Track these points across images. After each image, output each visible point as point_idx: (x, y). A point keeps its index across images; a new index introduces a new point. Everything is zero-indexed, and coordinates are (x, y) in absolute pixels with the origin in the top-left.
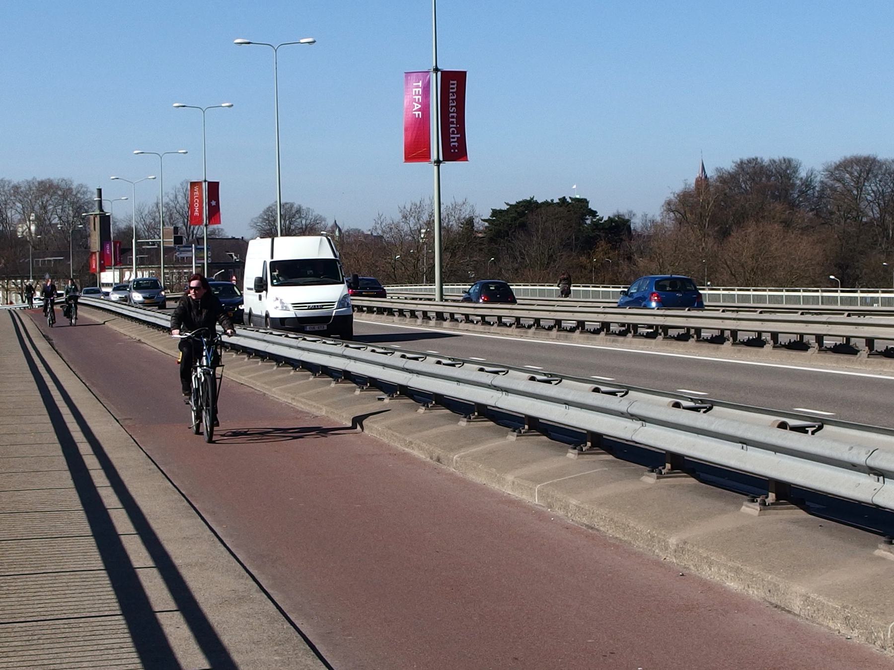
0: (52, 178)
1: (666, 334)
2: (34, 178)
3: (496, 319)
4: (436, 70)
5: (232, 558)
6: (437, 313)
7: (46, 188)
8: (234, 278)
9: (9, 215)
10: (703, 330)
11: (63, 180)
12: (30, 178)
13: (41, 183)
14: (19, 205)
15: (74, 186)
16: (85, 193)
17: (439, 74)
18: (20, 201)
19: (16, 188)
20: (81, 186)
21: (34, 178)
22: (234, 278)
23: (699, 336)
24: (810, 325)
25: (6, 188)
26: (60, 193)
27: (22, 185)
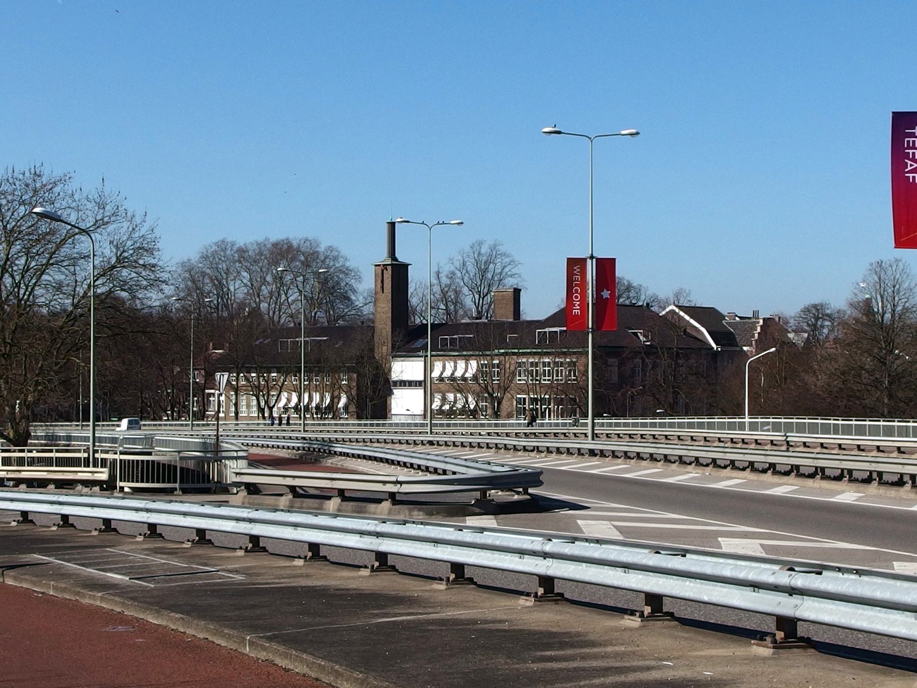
0: (291, 237)
1: (851, 476)
2: (267, 239)
3: (677, 458)
4: (592, 257)
5: (418, 573)
6: (590, 450)
7: (283, 252)
8: (745, 348)
9: (232, 288)
10: (884, 474)
11: (306, 240)
12: (260, 239)
13: (275, 245)
14: (245, 274)
15: (322, 249)
16: (335, 259)
17: (594, 260)
18: (248, 270)
19: (242, 251)
20: (331, 249)
21: (267, 239)
22: (745, 348)
23: (851, 476)
24: (906, 467)
25: (228, 252)
26: (302, 258)
27: (250, 247)
